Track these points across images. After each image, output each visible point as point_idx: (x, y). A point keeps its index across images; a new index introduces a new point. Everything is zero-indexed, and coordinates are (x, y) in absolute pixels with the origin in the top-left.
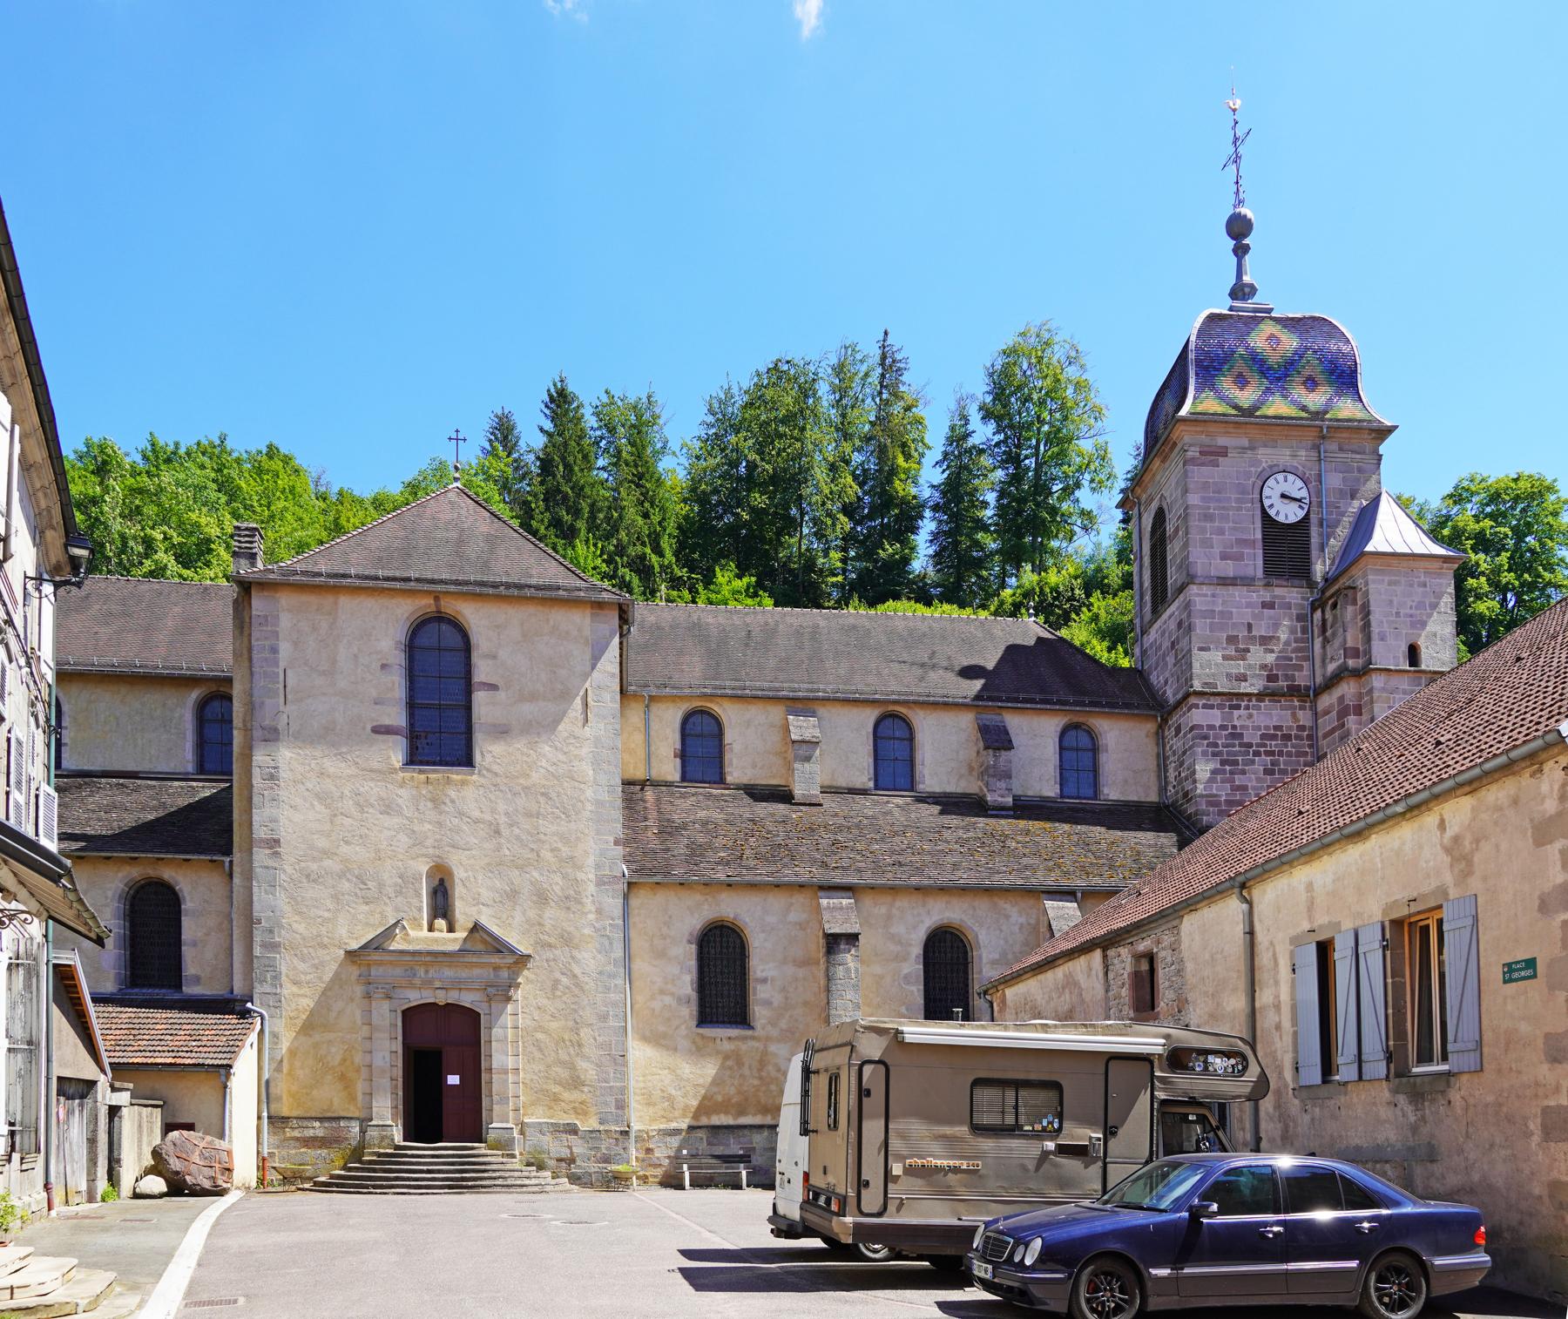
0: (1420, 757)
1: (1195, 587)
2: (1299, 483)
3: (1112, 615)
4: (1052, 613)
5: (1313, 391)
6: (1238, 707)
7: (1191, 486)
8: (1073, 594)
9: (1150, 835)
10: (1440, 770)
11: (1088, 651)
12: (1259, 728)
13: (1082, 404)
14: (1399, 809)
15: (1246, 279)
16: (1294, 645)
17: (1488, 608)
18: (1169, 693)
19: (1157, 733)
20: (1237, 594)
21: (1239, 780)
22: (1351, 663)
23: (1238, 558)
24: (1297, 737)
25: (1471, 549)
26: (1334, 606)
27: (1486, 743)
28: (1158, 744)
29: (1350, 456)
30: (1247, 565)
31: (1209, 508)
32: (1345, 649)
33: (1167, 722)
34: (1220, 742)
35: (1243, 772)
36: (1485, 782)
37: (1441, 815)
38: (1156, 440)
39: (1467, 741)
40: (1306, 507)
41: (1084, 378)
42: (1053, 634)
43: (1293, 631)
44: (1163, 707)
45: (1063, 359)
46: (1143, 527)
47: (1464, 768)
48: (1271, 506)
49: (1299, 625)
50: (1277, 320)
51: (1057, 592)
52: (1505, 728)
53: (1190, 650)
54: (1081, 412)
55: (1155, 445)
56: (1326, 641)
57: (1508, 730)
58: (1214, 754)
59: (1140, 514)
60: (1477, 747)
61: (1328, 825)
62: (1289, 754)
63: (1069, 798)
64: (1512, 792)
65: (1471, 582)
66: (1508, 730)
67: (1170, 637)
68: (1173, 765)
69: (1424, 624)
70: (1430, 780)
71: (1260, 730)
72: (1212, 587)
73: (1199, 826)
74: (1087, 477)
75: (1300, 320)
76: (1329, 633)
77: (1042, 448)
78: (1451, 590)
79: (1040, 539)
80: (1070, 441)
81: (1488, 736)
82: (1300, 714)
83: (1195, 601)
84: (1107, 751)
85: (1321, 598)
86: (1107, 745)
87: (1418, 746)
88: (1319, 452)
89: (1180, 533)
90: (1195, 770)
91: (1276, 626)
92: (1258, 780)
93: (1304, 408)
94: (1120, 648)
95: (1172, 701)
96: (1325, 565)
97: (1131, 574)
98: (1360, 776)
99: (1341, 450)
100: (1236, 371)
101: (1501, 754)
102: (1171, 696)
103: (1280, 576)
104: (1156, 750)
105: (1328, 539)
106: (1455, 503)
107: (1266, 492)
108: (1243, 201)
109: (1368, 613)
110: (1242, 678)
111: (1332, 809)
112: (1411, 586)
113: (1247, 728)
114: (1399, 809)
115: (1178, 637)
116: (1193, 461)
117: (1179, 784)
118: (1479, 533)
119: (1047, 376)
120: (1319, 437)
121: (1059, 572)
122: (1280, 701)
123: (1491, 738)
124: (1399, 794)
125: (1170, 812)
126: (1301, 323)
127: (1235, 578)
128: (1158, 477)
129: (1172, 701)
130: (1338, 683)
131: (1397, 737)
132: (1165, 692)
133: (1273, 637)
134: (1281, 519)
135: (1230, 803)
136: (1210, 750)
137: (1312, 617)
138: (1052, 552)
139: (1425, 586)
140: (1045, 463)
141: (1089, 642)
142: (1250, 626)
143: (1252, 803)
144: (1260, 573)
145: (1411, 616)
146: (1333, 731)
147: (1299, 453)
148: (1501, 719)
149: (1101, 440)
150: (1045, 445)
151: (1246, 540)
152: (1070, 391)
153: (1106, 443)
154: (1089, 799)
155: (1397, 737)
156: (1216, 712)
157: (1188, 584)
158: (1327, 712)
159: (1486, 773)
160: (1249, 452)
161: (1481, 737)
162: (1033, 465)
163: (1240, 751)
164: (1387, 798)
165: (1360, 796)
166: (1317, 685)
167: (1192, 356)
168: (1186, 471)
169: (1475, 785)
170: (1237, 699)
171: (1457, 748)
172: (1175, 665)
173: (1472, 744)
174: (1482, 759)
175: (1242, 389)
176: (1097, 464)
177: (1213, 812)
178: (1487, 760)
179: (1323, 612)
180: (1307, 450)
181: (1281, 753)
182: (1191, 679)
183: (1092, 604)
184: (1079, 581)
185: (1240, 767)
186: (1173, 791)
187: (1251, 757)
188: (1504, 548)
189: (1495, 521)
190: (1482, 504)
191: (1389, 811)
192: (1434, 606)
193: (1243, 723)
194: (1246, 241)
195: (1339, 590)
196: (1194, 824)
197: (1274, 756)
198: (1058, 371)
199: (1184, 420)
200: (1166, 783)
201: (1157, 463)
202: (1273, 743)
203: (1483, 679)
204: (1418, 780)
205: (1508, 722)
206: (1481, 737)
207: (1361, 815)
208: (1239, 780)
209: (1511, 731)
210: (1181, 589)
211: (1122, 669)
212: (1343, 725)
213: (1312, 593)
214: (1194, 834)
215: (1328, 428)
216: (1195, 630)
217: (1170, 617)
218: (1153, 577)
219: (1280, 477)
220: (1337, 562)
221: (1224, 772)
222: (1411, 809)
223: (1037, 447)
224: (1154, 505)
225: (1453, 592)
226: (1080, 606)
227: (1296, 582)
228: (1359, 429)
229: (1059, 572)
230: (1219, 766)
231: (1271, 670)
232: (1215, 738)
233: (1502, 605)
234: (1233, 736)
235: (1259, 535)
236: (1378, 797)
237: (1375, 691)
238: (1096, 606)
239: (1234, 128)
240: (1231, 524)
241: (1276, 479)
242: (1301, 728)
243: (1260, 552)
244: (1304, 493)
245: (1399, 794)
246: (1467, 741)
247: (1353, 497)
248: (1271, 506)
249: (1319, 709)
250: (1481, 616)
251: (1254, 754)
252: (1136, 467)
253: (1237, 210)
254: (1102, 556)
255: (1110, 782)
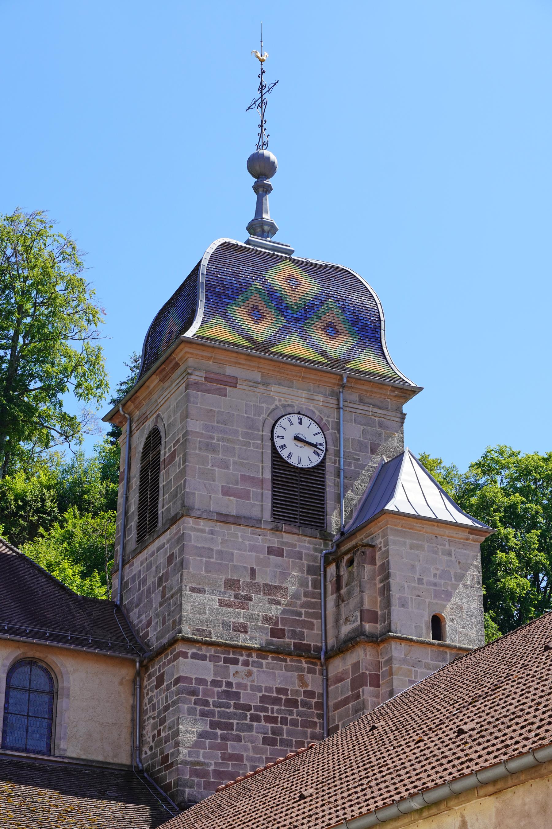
0: (440, 745)
1: (190, 520)
2: (315, 428)
3: (90, 536)
4: (15, 524)
5: (333, 338)
6: (235, 662)
7: (193, 411)
8: (43, 506)
9: (116, 806)
10: (462, 763)
11: (54, 574)
12: (259, 689)
13: (74, 304)
14: (415, 804)
15: (266, 217)
16: (304, 599)
17: (518, 585)
18: (152, 635)
19: (134, 681)
20: (239, 534)
21: (232, 747)
22: (368, 627)
23: (245, 495)
24: (305, 704)
25: (500, 521)
26: (351, 562)
27: (512, 738)
28: (134, 695)
29: (371, 409)
30: (252, 505)
31: (212, 438)
32: (362, 611)
33: (147, 669)
34: (211, 700)
35: (238, 739)
36: (510, 783)
37: (462, 816)
38: (156, 357)
39: (491, 733)
40: (322, 454)
41: (79, 276)
42: (12, 550)
43: (303, 583)
44: (143, 651)
45: (56, 253)
46: (133, 446)
47: (487, 764)
48: (283, 447)
49: (310, 577)
50: (295, 261)
51: (23, 500)
52: (532, 723)
53: (180, 589)
54: (71, 311)
55: (153, 362)
56: (340, 600)
57: (535, 726)
58: (203, 714)
59: (131, 431)
60: (502, 741)
61: (334, 815)
62: (294, 723)
63: (12, 749)
64: (540, 798)
65: (500, 555)
66: (535, 726)
67: (157, 572)
68: (152, 721)
69: (449, 596)
70: (450, 774)
71: (261, 691)
72: (211, 523)
73: (180, 799)
74: (73, 380)
75: (321, 267)
76: (344, 591)
77: (21, 340)
78: (478, 562)
79: (7, 438)
80: (55, 338)
81: (514, 731)
82: (309, 677)
83: (190, 535)
84: (68, 696)
85: (336, 552)
86: (68, 689)
87: (439, 732)
88: (338, 400)
89: (177, 459)
90: (178, 730)
91: (284, 575)
92: (256, 749)
93: (323, 353)
94: (96, 574)
95: (155, 645)
96: (341, 517)
97: (115, 493)
98: (373, 759)
99: (361, 401)
100: (251, 303)
101: (528, 753)
102: (154, 639)
103: (289, 521)
104: (131, 701)
105: (346, 491)
106: (484, 472)
107: (278, 431)
108: (267, 144)
109: (388, 576)
110: (242, 629)
111: (338, 797)
112: (436, 553)
113: (245, 687)
114: (415, 804)
115: (167, 572)
116: (196, 386)
117: (157, 746)
118: (510, 507)
119: (35, 267)
120: (338, 385)
121: (28, 478)
122: (285, 661)
123: (518, 733)
124: (415, 787)
125: (144, 778)
126: (323, 271)
127: (238, 517)
128: (155, 396)
129: (155, 645)
130: (353, 647)
131: (417, 718)
132: (147, 634)
133: (280, 587)
134: (294, 461)
135: (219, 774)
136: (199, 708)
137: (325, 571)
138: (21, 455)
139: (450, 554)
140: (23, 357)
141: (58, 564)
142: (253, 572)
143: (246, 777)
144: (267, 515)
145: (435, 585)
146: (346, 701)
147: (316, 398)
148: (528, 713)
149: (93, 344)
150: (24, 337)
151: (253, 478)
152: (60, 287)
153: (99, 349)
154: (39, 753)
155: (417, 718)
156: (208, 664)
157: (182, 516)
158: (339, 679)
159: (512, 773)
160: (261, 387)
161: (507, 731)
162: (8, 357)
163: (235, 714)
164: (402, 789)
165: (346, 805)
166: (329, 648)
167: (202, 279)
168: (188, 395)
169: (499, 786)
170: (234, 653)
171: (481, 740)
172: (161, 604)
173: (496, 738)
174: (507, 757)
175: (256, 322)
176: (86, 368)
177: (199, 784)
178: (512, 758)
179: (338, 568)
180: (325, 395)
181: (284, 721)
182: (180, 623)
183: (66, 520)
184: (52, 492)
185: (234, 732)
186: (149, 753)
187: (248, 721)
188: (534, 526)
189: (527, 498)
190: (512, 479)
191: (404, 806)
192: (460, 577)
193: (240, 681)
194: (269, 182)
195: (355, 547)
196: (173, 796)
197: (276, 723)
198: (49, 265)
199: (189, 342)
200: (142, 743)
201: (155, 381)
202: (276, 708)
203: (510, 665)
204: (437, 773)
205: (535, 716)
206: (507, 731)
207: (372, 807)
208: (232, 747)
209: (539, 728)
210: (174, 520)
211: (95, 601)
212: (358, 696)
213: (326, 545)
214: (173, 809)
215: (348, 377)
216: (188, 568)
217: (159, 549)
218: (142, 501)
219: (295, 418)
220: (354, 516)
221: (215, 736)
222: (429, 806)
223: (15, 339)
224: (148, 425)
225: (480, 565)
226: (51, 521)
227: (309, 531)
228: (381, 385)
229: (28, 478)
230: (208, 729)
231: (276, 623)
232: (205, 693)
233: (532, 585)
234: (227, 694)
235: (268, 475)
236: (392, 788)
237: (394, 662)
238: (70, 522)
239: (260, 76)
240: (236, 459)
241: (289, 420)
242: (310, 694)
243: (268, 493)
244: (320, 439)
245: (415, 787)
246: (491, 733)
247: (373, 452)
248: (283, 447)
249: (331, 674)
250: (512, 593)
251: (252, 720)
252: (132, 379)
253: (261, 151)
254: (83, 469)
255: (69, 734)
